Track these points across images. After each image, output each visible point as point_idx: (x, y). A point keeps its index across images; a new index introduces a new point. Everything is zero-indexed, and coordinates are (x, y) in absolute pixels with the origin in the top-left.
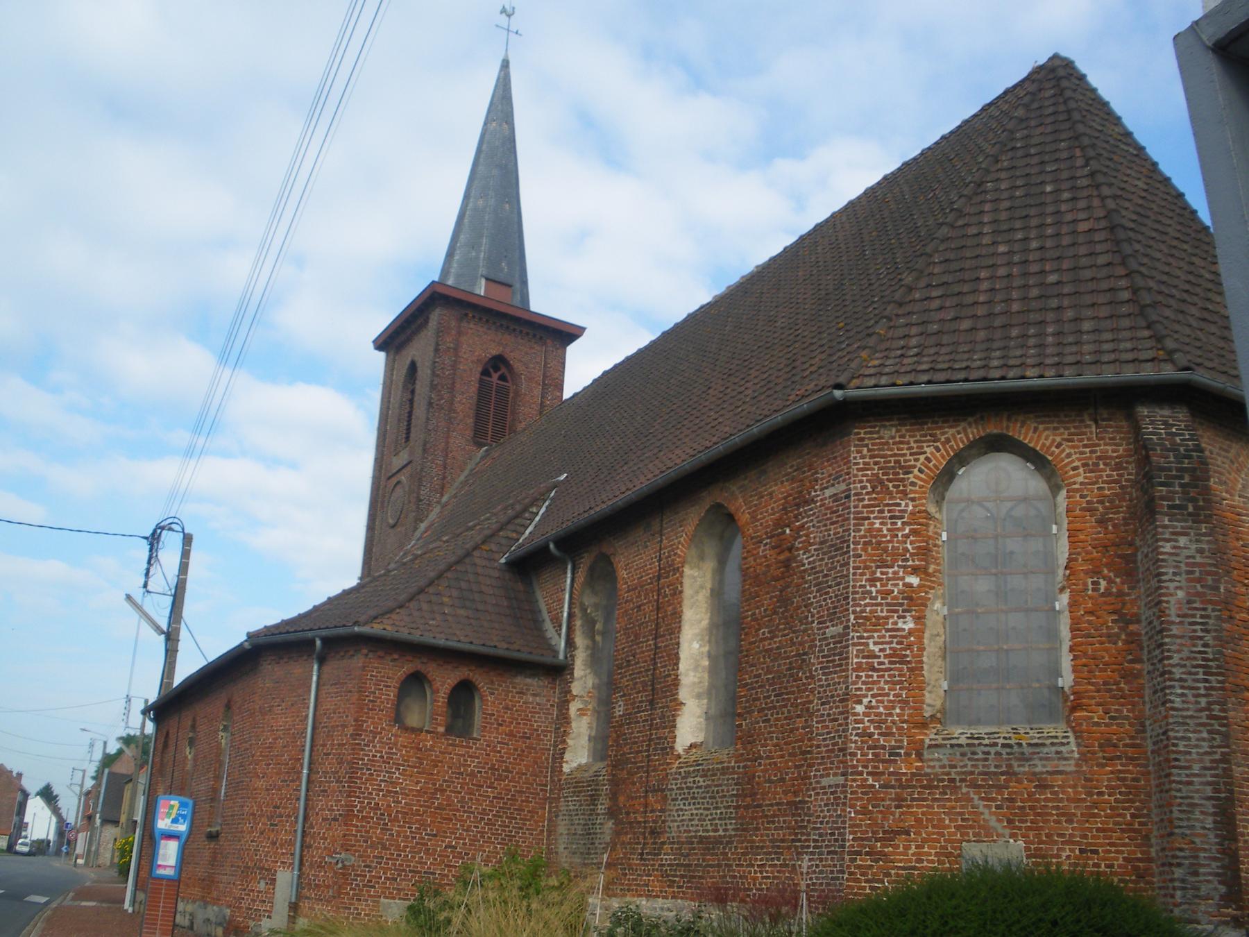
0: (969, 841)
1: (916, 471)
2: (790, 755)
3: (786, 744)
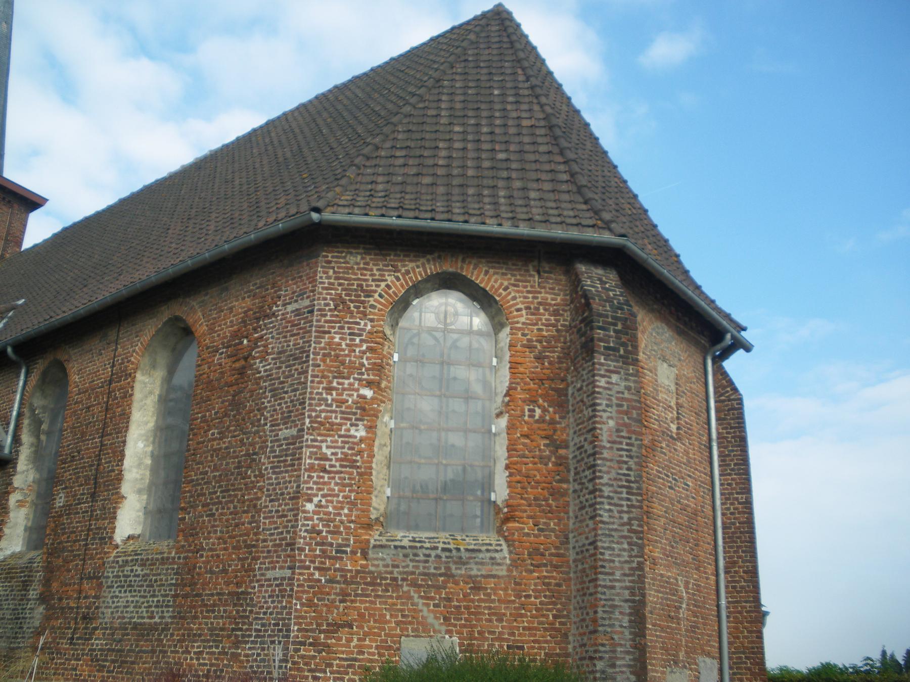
0: (408, 636)
1: (376, 296)
2: (234, 548)
3: (230, 537)
